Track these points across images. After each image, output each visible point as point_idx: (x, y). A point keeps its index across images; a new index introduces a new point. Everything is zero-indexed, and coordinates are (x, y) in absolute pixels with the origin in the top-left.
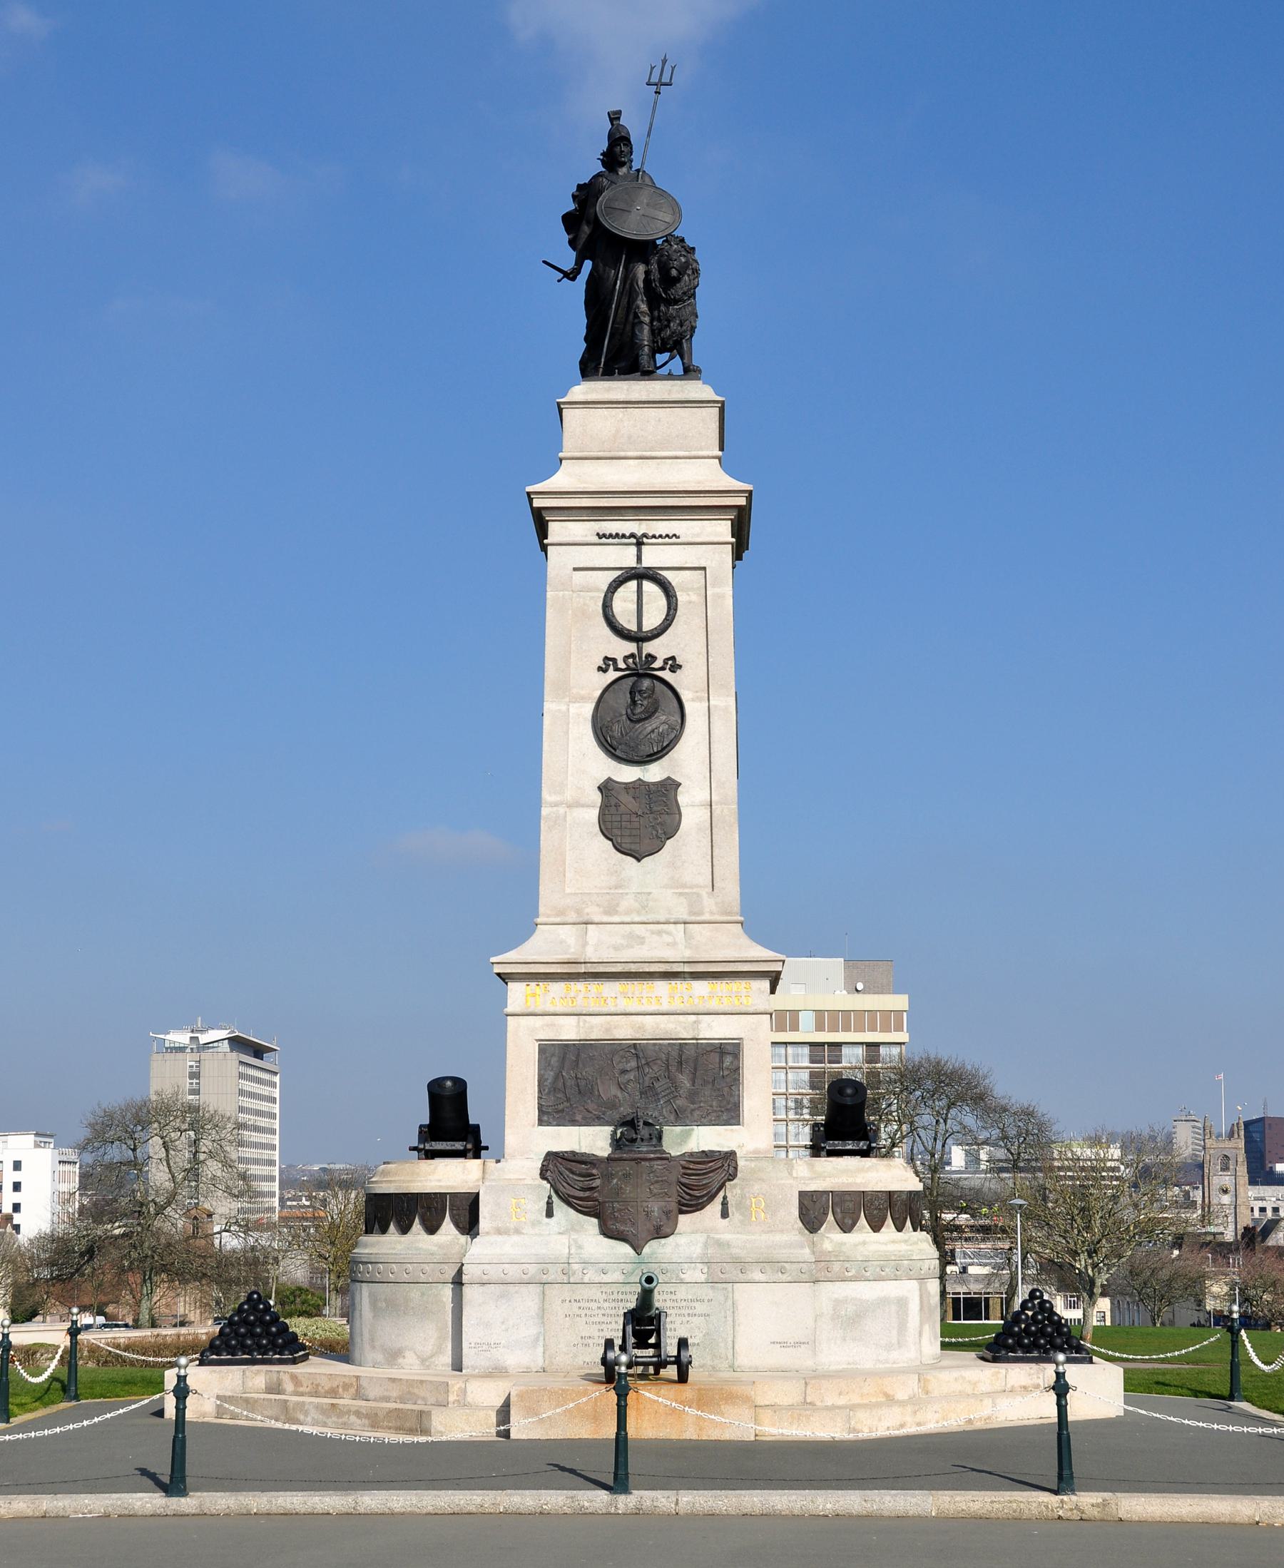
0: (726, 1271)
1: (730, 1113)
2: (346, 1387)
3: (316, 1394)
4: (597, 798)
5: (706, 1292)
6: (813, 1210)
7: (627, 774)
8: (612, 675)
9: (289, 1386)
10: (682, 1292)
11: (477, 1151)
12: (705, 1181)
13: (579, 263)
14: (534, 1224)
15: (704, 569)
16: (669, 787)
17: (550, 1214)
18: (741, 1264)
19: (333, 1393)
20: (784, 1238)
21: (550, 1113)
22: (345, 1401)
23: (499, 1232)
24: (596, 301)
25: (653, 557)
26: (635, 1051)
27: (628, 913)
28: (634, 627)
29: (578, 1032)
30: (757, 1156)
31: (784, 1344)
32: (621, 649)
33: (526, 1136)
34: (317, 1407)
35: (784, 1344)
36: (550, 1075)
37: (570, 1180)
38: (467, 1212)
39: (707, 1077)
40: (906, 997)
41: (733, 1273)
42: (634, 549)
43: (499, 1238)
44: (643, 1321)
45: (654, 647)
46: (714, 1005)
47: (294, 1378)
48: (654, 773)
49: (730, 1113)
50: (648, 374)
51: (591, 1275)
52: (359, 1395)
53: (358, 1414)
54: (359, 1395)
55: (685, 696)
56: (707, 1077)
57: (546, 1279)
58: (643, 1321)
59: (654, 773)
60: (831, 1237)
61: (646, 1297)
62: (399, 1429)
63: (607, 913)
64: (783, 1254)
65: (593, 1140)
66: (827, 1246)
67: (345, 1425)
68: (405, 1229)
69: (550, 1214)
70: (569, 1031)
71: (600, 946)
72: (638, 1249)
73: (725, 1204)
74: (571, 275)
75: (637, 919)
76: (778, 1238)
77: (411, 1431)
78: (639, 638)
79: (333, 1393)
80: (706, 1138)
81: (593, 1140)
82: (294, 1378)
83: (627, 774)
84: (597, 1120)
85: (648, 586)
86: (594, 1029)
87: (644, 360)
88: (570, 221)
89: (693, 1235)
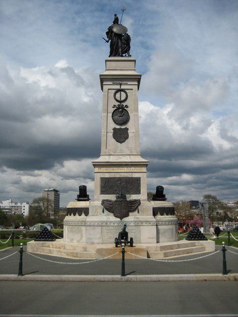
0: (139, 224)
1: (138, 192)
2: (62, 247)
3: (56, 248)
4: (112, 131)
5: (135, 228)
6: (156, 211)
7: (118, 127)
8: (115, 108)
9: (51, 246)
10: (130, 228)
11: (88, 200)
12: (134, 206)
13: (109, 40)
14: (100, 214)
15: (135, 61)
16: (127, 129)
17: (103, 212)
18: (142, 222)
19: (59, 248)
20: (150, 217)
21: (104, 191)
22: (62, 250)
23: (93, 215)
24: (112, 46)
25: (123, 87)
26: (120, 179)
27: (118, 153)
28: (119, 99)
29: (90, 191)
30: (144, 200)
31: (150, 238)
32: (117, 104)
33: (96, 201)
34: (56, 251)
35: (150, 238)
36: (103, 184)
37: (108, 207)
38: (86, 211)
39: (134, 185)
40: (60, 207)
41: (140, 224)
42: (119, 86)
43: (93, 217)
44: (124, 235)
45: (125, 104)
46: (135, 171)
47: (52, 245)
48: (123, 127)
49: (138, 192)
50: (122, 56)
51: (112, 224)
52: (64, 248)
53: (64, 253)
54: (64, 248)
55: (129, 112)
56: (134, 185)
57: (103, 225)
58: (124, 235)
59: (123, 127)
60: (159, 217)
61: (125, 229)
62: (72, 256)
63: (114, 153)
64: (150, 220)
65: (112, 197)
66: (158, 218)
67: (62, 255)
68: (75, 215)
69: (103, 212)
70: (107, 176)
71: (113, 159)
72: (121, 219)
73: (138, 210)
74: (108, 42)
75: (137, 171)
76: (148, 217)
77: (75, 257)
78: (121, 102)
79: (59, 248)
80: (134, 197)
81: (112, 197)
82: (52, 245)
83: (118, 127)
84: (113, 194)
85: (122, 93)
86: (112, 175)
87: (120, 54)
88: (107, 33)
89: (131, 218)
